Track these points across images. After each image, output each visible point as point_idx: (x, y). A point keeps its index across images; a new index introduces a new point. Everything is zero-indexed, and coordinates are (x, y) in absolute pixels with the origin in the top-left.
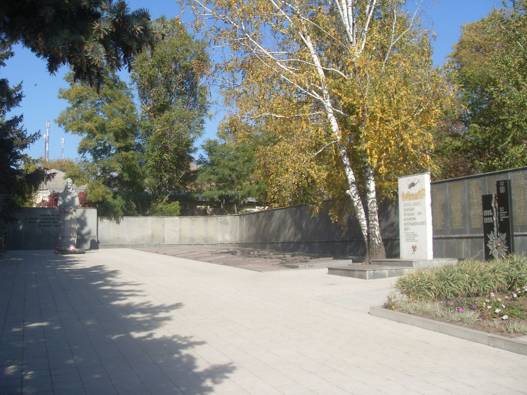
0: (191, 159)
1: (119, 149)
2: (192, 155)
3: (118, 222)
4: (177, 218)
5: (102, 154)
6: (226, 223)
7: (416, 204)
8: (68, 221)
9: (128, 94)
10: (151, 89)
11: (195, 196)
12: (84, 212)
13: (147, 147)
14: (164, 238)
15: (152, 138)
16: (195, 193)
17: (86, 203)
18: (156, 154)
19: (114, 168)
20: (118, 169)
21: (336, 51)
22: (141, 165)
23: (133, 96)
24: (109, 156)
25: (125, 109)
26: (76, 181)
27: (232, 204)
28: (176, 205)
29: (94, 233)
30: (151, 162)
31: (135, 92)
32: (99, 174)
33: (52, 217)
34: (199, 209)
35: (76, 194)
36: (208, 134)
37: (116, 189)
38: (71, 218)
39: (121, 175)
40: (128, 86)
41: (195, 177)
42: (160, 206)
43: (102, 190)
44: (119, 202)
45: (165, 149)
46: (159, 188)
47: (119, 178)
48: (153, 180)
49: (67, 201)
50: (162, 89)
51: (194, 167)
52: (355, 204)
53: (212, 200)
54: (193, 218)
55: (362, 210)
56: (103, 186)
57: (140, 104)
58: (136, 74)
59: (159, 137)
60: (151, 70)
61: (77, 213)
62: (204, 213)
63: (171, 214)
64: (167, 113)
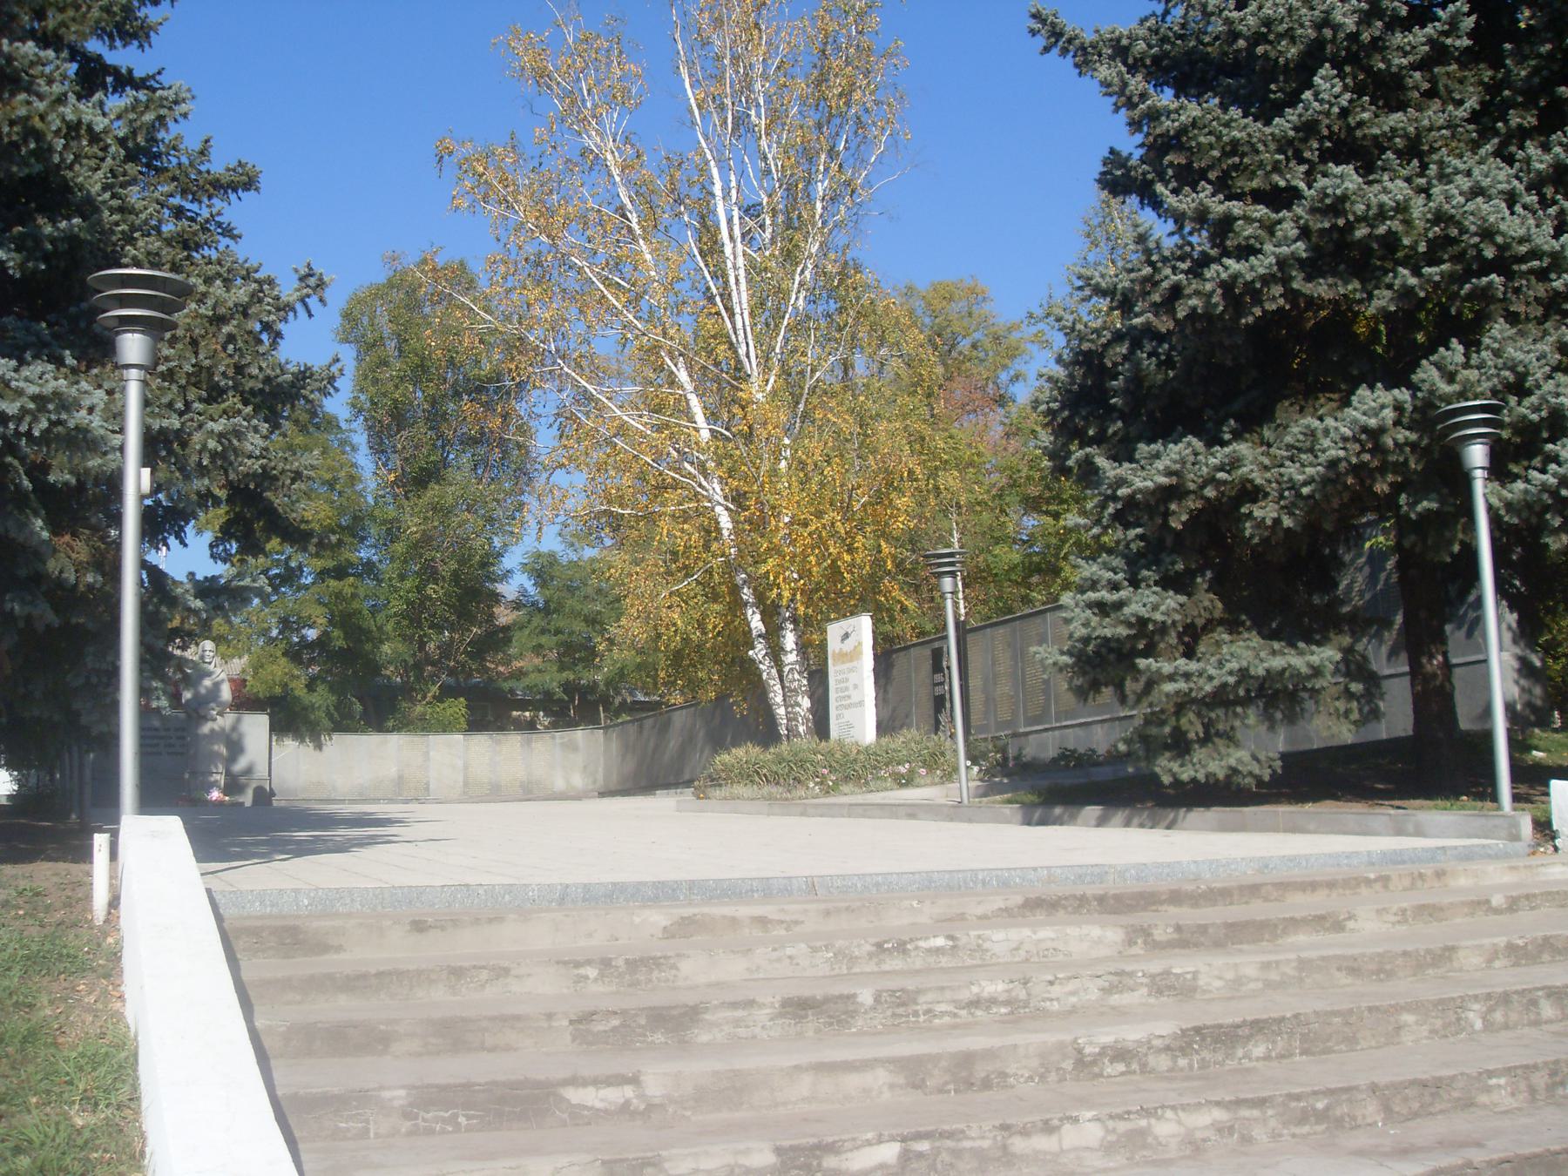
0: (496, 598)
1: (322, 574)
2: (501, 588)
3: (319, 747)
4: (459, 737)
5: (281, 585)
6: (572, 747)
7: (851, 670)
8: (205, 736)
9: (343, 443)
10: (399, 431)
11: (506, 686)
12: (238, 720)
13: (388, 569)
14: (427, 784)
15: (399, 547)
16: (506, 679)
17: (245, 702)
18: (408, 584)
19: (310, 617)
20: (320, 621)
21: (724, 383)
22: (374, 611)
23: (354, 449)
24: (299, 589)
25: (335, 479)
26: (223, 648)
27: (595, 705)
28: (457, 707)
29: (261, 770)
30: (397, 606)
31: (361, 438)
32: (275, 633)
33: (163, 733)
34: (517, 719)
35: (223, 676)
36: (534, 540)
37: (315, 669)
38: (212, 731)
39: (325, 634)
40: (344, 425)
41: (507, 641)
42: (419, 709)
43: (281, 668)
44: (321, 698)
45: (430, 573)
46: (418, 667)
47: (322, 642)
48: (401, 647)
49: (203, 691)
50: (422, 431)
51: (504, 616)
52: (765, 676)
53: (548, 694)
54: (497, 736)
55: (778, 688)
56: (283, 661)
57: (372, 467)
58: (363, 397)
59: (415, 546)
60: (397, 387)
61: (224, 721)
62: (531, 726)
63: (445, 727)
64: (433, 490)
